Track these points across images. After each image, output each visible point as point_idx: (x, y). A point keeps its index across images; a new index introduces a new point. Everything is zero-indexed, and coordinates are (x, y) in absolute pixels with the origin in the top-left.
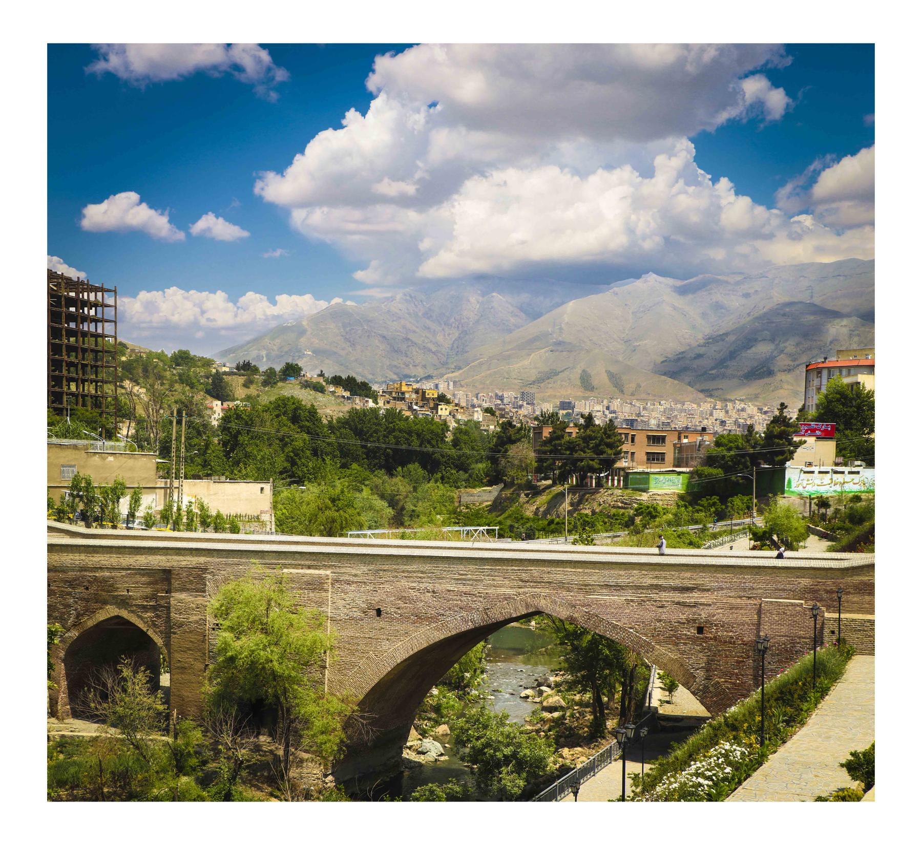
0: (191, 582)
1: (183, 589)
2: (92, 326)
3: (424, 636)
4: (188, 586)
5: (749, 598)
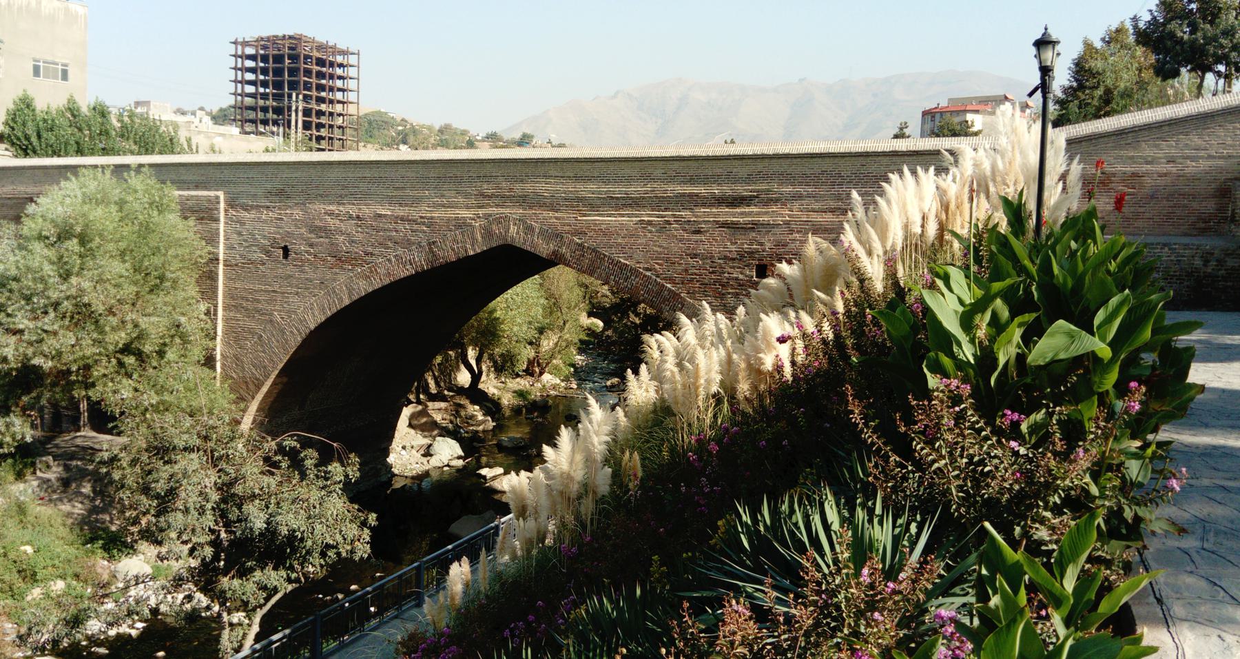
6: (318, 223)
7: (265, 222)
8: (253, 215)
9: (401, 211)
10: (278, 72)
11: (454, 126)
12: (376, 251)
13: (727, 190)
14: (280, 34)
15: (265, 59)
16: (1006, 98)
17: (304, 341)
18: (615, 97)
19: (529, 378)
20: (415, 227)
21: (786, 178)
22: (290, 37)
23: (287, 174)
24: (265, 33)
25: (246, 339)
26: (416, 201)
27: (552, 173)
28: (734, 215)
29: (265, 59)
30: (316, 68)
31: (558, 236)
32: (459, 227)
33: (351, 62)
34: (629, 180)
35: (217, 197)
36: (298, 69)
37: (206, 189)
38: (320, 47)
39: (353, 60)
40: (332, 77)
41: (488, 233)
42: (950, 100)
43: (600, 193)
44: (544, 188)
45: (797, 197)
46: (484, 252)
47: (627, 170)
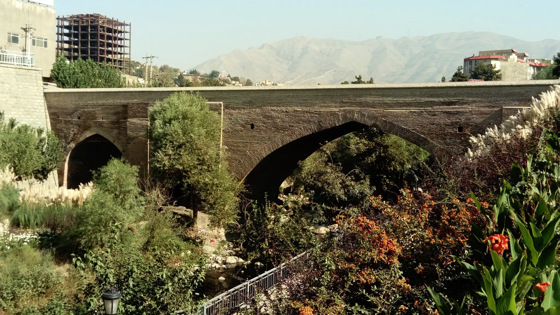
0: (139, 112)
1: (134, 116)
2: (119, 48)
3: (281, 140)
4: (137, 115)
5: (494, 107)
6: (267, 114)
7: (243, 114)
8: (237, 111)
9: (306, 109)
10: (84, 36)
11: (170, 66)
12: (295, 125)
13: (446, 99)
14: (85, 14)
15: (76, 28)
16: (513, 51)
17: (260, 162)
18: (262, 47)
19: (295, 196)
20: (313, 115)
21: (471, 95)
22: (91, 16)
23: (253, 95)
24: (76, 12)
25: (233, 162)
26: (314, 105)
27: (373, 93)
28: (449, 109)
29: (76, 28)
30: (106, 34)
31: (376, 118)
32: (332, 115)
33: (126, 30)
34: (406, 96)
35: (221, 104)
36: (97, 34)
37: (214, 101)
38: (110, 21)
39: (127, 29)
40: (115, 39)
41: (345, 117)
42: (480, 52)
43: (393, 101)
44: (369, 99)
45: (475, 102)
46: (343, 125)
47: (405, 92)
